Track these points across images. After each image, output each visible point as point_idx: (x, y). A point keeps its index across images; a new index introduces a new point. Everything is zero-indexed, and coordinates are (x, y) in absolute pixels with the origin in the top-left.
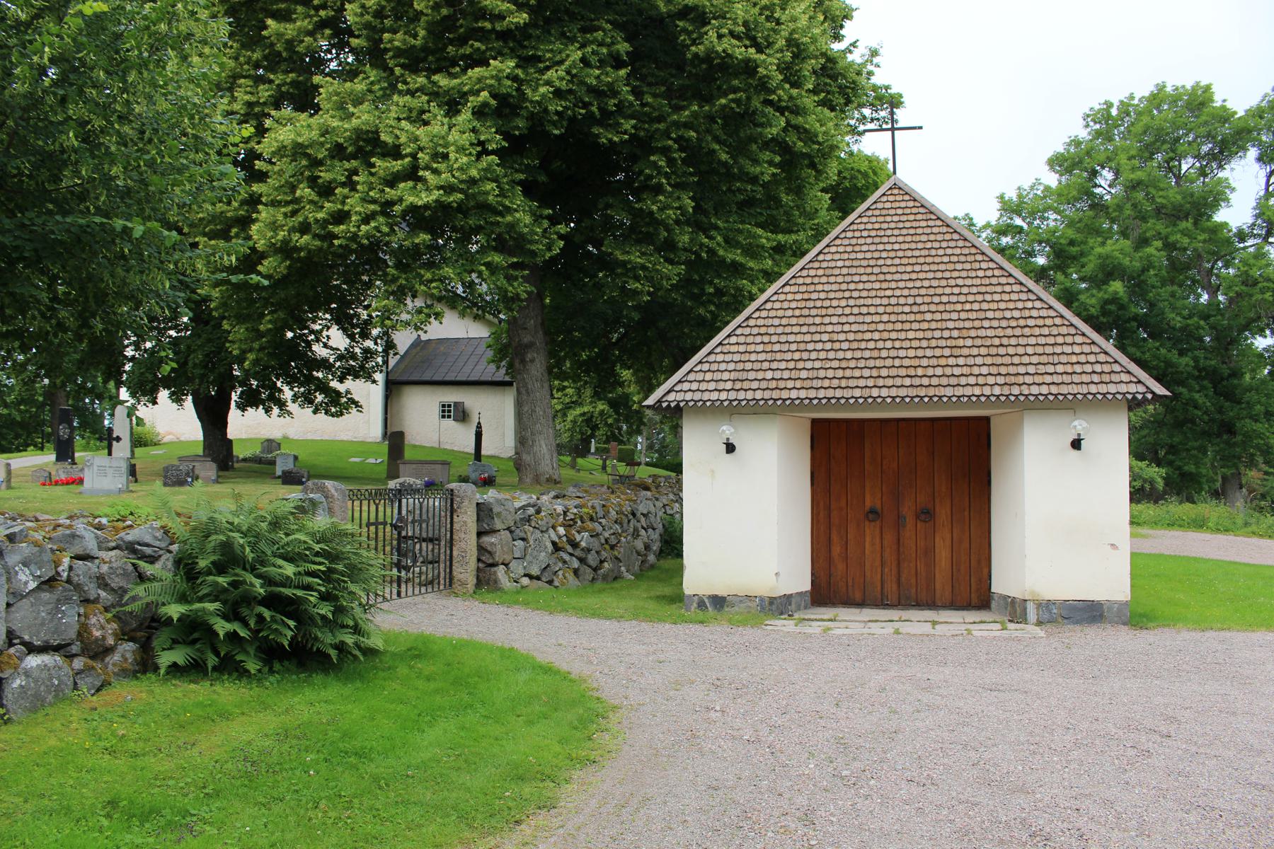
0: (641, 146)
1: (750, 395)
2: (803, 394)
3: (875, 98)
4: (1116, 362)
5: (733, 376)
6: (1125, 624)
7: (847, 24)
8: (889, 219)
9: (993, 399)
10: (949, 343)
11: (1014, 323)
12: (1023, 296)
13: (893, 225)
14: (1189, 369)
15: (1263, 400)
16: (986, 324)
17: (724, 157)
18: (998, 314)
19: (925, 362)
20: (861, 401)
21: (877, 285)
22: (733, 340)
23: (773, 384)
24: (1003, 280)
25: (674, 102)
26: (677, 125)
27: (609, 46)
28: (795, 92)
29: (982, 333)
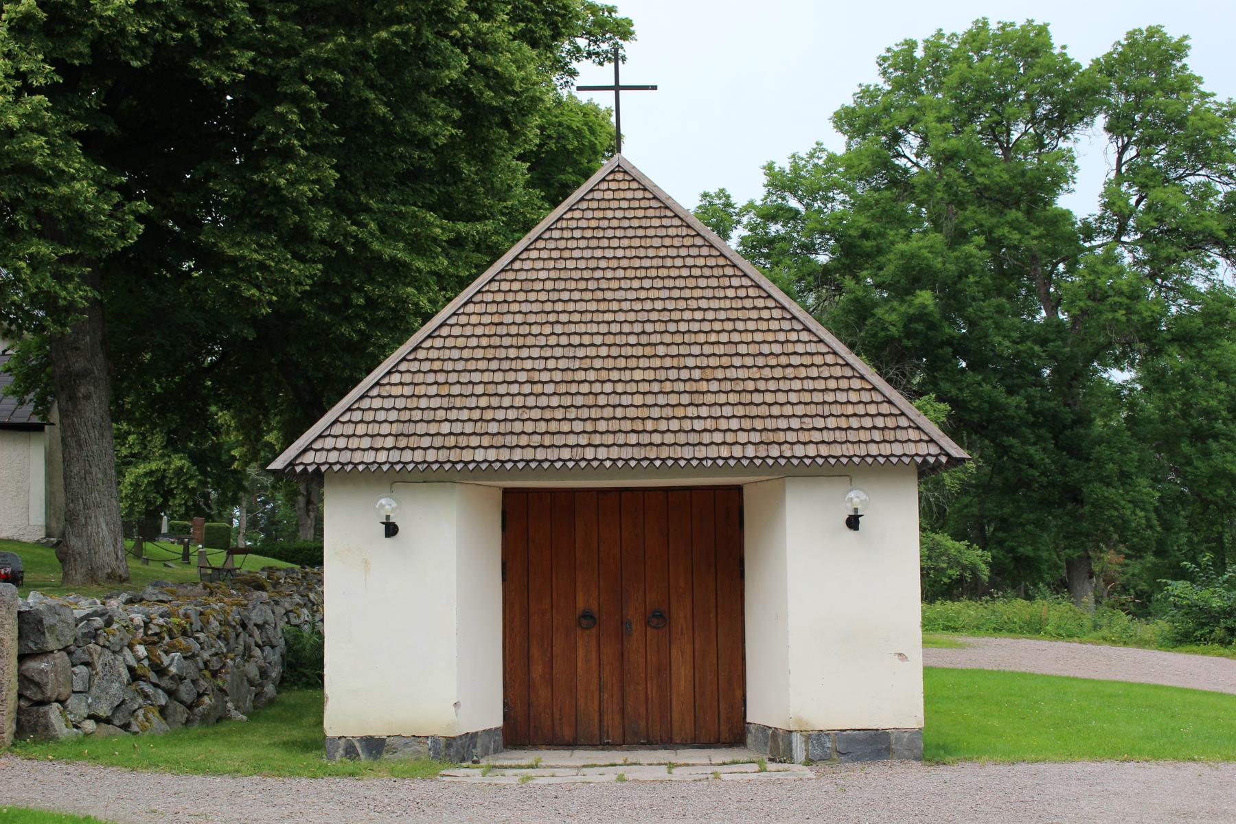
0: (261, 89)
1: (418, 456)
2: (492, 455)
3: (595, 23)
4: (903, 414)
5: (396, 428)
6: (917, 759)
8: (609, 214)
10: (689, 386)
11: (773, 362)
13: (615, 223)
15: (1116, 456)
16: (737, 361)
17: (382, 110)
18: (753, 349)
19: (656, 413)
20: (571, 464)
21: (593, 306)
22: (396, 378)
23: (451, 441)
24: (760, 303)
25: (310, 28)
26: (315, 62)
28: (484, 26)
29: (731, 373)
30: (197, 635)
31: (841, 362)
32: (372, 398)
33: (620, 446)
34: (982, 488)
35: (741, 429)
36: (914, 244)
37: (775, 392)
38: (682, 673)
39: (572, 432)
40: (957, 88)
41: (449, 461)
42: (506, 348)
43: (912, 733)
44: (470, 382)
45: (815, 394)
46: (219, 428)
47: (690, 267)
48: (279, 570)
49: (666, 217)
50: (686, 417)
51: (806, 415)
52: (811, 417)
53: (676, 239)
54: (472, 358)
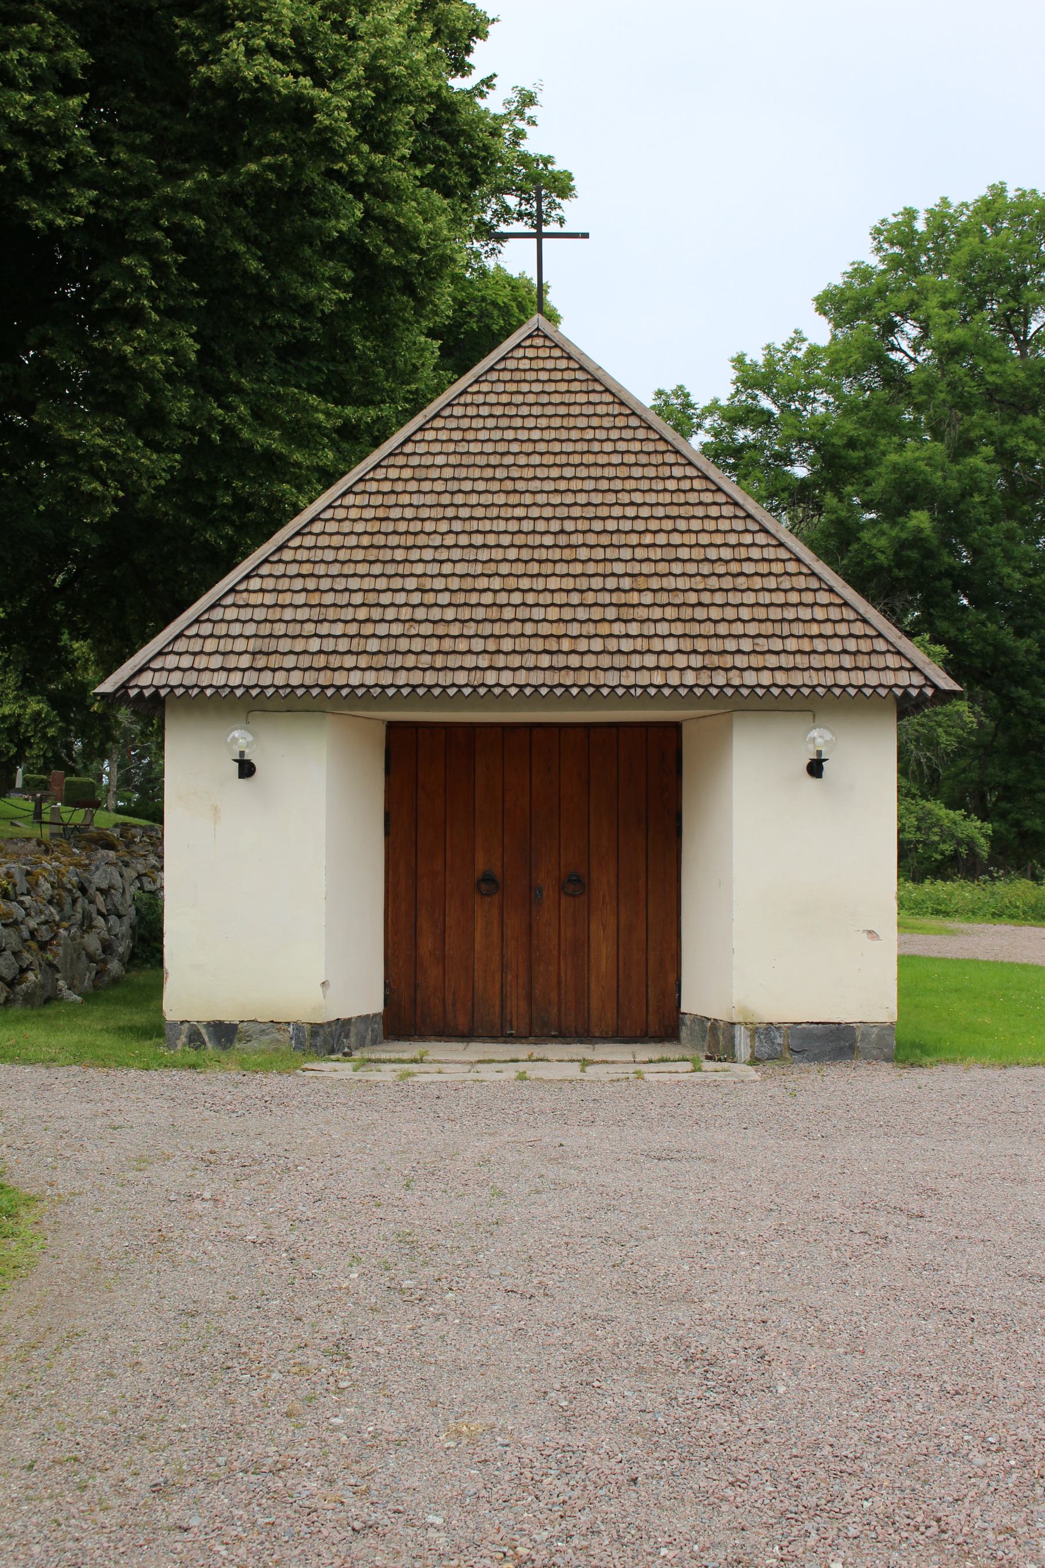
0: (107, 237)
1: (280, 679)
2: (370, 678)
3: (527, 177)
4: (880, 635)
5: (253, 645)
6: (887, 1060)
7: (478, 45)
8: (525, 387)
9: (683, 692)
10: (616, 598)
11: (721, 569)
12: (739, 525)
13: (531, 398)
14: (1033, 658)
16: (677, 568)
17: (254, 265)
18: (697, 553)
19: (574, 629)
20: (467, 691)
21: (501, 499)
22: (255, 584)
23: (321, 661)
24: (707, 498)
25: (166, 163)
26: (170, 203)
27: (50, 52)
28: (378, 158)
29: (669, 583)
30: (22, 898)
31: (805, 570)
32: (225, 607)
33: (529, 669)
34: (981, 749)
35: (679, 651)
36: (909, 455)
37: (722, 606)
38: (603, 951)
39: (470, 652)
40: (966, 267)
41: (317, 685)
42: (393, 548)
43: (883, 1029)
44: (346, 590)
45: (772, 609)
46: (74, 662)
47: (623, 453)
48: (135, 826)
49: (594, 391)
50: (611, 635)
51: (759, 636)
52: (767, 637)
53: (606, 419)
54: (350, 561)
